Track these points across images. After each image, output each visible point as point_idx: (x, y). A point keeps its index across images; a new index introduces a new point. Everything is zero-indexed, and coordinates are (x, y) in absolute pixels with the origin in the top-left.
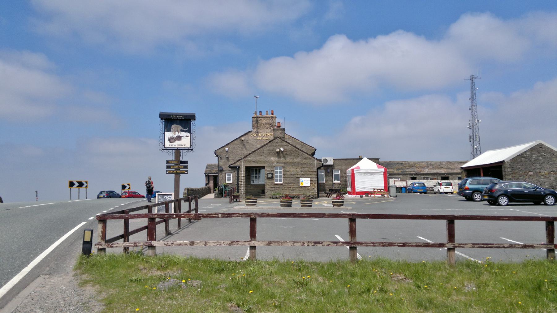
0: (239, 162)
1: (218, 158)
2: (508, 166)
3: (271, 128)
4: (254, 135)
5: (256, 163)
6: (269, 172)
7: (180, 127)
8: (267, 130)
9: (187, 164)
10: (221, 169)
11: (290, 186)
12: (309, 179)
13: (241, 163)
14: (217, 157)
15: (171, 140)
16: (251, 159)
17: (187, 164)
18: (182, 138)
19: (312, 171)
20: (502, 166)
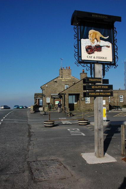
7: (99, 35)
8: (67, 76)
9: (84, 86)
15: (90, 50)
17: (84, 86)
18: (102, 48)
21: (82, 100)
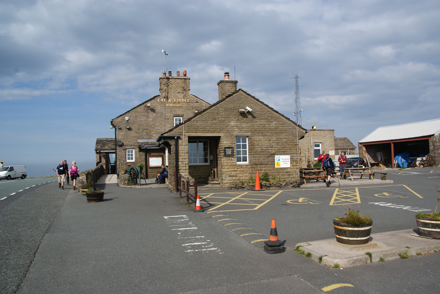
0: (178, 128)
1: (116, 130)
2: (438, 141)
3: (183, 93)
4: (162, 100)
5: (206, 131)
6: (227, 146)
8: (179, 95)
10: (121, 144)
11: (260, 167)
12: (288, 157)
13: (181, 131)
14: (114, 129)
16: (199, 123)
19: (292, 144)
20: (429, 141)
21: (226, 155)
